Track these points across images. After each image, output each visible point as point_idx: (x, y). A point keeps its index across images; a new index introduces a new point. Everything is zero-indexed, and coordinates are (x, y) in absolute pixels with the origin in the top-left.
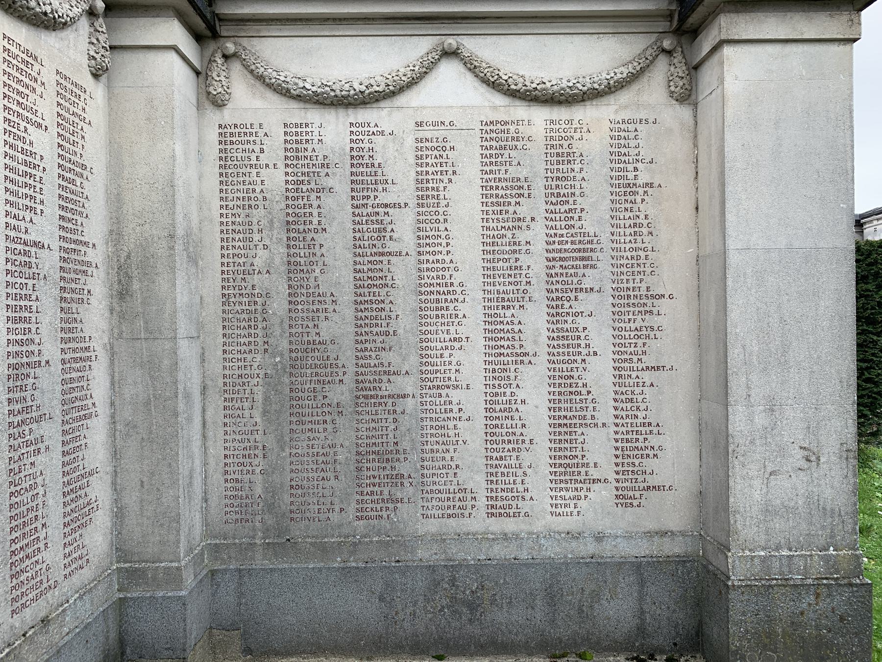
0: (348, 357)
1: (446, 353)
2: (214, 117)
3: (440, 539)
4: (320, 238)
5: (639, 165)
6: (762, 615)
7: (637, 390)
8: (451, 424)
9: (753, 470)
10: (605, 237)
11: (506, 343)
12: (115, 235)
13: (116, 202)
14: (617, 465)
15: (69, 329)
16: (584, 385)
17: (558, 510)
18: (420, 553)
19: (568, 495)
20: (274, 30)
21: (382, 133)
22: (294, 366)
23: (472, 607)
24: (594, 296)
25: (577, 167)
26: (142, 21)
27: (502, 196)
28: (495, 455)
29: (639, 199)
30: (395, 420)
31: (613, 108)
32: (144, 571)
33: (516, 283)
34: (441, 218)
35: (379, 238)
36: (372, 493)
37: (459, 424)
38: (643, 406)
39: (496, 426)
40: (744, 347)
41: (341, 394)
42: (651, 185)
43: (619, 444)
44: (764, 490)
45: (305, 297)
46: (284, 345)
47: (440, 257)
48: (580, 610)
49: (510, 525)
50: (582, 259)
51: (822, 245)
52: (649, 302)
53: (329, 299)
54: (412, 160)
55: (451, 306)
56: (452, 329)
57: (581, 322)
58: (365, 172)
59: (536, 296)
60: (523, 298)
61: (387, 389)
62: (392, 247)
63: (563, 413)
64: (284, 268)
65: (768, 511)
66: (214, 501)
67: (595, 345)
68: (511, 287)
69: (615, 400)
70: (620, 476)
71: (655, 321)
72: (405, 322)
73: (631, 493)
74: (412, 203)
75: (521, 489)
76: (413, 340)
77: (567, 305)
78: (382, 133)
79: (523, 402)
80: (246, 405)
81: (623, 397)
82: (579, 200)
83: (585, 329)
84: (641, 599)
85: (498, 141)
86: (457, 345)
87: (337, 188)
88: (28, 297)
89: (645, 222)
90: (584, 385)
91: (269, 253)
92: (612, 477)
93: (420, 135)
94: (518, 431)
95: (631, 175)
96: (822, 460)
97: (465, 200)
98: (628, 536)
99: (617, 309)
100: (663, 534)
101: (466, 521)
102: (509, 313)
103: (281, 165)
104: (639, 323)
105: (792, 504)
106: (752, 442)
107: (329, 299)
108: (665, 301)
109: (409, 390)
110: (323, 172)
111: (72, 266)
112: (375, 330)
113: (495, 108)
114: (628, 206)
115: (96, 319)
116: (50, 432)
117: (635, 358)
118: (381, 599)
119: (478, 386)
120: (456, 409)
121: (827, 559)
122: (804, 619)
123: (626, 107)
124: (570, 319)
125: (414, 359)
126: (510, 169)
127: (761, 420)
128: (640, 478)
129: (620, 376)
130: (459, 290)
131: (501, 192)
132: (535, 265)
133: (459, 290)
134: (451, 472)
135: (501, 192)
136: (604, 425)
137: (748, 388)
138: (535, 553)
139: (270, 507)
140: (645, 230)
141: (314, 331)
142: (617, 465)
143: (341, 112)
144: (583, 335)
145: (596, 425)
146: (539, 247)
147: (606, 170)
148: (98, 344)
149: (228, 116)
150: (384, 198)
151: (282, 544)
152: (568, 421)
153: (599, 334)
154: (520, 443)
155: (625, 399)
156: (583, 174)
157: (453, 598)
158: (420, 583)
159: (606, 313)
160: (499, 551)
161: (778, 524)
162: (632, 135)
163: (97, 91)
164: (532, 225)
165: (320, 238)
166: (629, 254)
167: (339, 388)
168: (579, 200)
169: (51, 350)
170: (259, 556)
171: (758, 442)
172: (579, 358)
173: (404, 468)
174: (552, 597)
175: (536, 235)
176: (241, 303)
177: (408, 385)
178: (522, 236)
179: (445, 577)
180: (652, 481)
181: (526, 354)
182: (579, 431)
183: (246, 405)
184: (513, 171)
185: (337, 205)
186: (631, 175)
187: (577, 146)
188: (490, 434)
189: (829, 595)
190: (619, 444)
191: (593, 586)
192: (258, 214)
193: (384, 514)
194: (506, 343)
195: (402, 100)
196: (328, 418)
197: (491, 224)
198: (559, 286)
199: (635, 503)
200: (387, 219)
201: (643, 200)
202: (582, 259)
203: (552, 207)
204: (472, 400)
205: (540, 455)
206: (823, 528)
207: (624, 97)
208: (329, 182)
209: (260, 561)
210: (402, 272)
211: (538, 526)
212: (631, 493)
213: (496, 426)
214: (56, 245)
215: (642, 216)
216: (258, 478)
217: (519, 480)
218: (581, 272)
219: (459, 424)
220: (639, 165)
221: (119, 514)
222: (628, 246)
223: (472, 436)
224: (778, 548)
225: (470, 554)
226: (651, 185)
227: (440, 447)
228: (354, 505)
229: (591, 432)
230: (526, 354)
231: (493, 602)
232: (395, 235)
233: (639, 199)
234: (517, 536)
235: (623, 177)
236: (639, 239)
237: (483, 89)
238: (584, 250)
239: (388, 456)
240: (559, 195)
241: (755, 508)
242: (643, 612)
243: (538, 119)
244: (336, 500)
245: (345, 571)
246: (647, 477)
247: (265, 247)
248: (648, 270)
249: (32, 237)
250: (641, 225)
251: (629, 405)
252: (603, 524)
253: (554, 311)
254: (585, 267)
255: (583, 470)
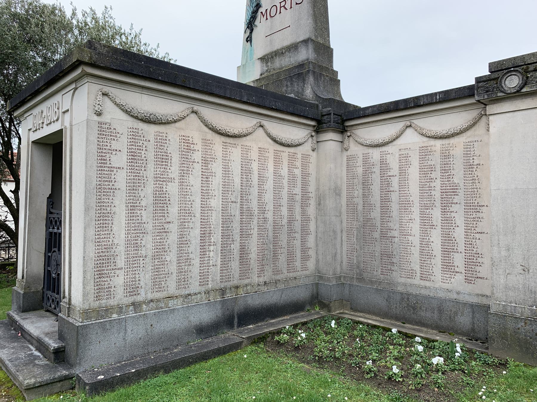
0: (378, 224)
1: (408, 224)
2: (346, 154)
3: (405, 285)
4: (371, 187)
5: (475, 157)
6: (501, 326)
7: (474, 241)
8: (409, 247)
9: (501, 271)
10: (462, 185)
11: (427, 221)
12: (318, 189)
13: (318, 180)
14: (465, 267)
15: (304, 213)
16: (454, 238)
17: (444, 281)
18: (399, 288)
19: (447, 276)
20: (360, 127)
21: (389, 154)
22: (364, 226)
23: (414, 309)
24: (458, 205)
25: (451, 160)
26: (324, 134)
27: (426, 171)
28: (423, 259)
29: (474, 170)
30: (392, 245)
31: (465, 137)
32: (323, 277)
33: (430, 201)
34: (406, 179)
35: (388, 186)
36: (385, 267)
37: (412, 248)
38: (476, 247)
39: (423, 250)
40: (497, 225)
41: (377, 235)
42: (479, 165)
43: (466, 260)
44: (505, 280)
45: (368, 206)
46: (362, 219)
47: (405, 192)
48: (450, 318)
49: (428, 284)
50: (453, 192)
51: (530, 187)
52: (478, 208)
53: (373, 206)
54: (398, 161)
55: (409, 208)
56: (409, 216)
57: (453, 215)
58: (384, 165)
59: (437, 205)
60: (433, 206)
61: (390, 234)
62: (391, 189)
63: (446, 247)
64: (362, 196)
65: (506, 287)
66: (344, 263)
67: (458, 223)
68: (429, 202)
69: (465, 244)
70: (466, 272)
71: (480, 215)
72: (395, 213)
73: (471, 279)
74: (398, 175)
75: (431, 272)
76: (398, 219)
77: (448, 208)
78: (389, 154)
79: (432, 242)
80: (352, 236)
81: (468, 243)
82: (452, 171)
83: (454, 217)
84: (473, 318)
85: (425, 153)
86: (411, 221)
87: (376, 172)
88: (292, 206)
89: (477, 178)
90: (454, 238)
91: (358, 192)
92: (464, 272)
93: (400, 153)
94: (431, 252)
95: (471, 161)
96: (530, 271)
97: (414, 173)
98: (470, 294)
99: (466, 210)
100: (483, 296)
101: (413, 280)
102: (428, 211)
103: (362, 166)
104: (474, 216)
105: (517, 287)
106: (501, 261)
107: (373, 206)
108: (485, 208)
109: (396, 235)
110: (373, 167)
111: (305, 198)
112: (386, 215)
113: (424, 142)
114: (470, 172)
115: (311, 210)
116: (298, 236)
117: (473, 229)
118: (387, 300)
119: (418, 236)
120: (410, 243)
121: (532, 310)
122: (520, 331)
123: (469, 137)
124: (449, 214)
125: (398, 225)
126: (429, 162)
127: (504, 253)
128: (475, 273)
129: (467, 235)
130: (412, 203)
131: (425, 170)
132: (437, 194)
133: (412, 203)
134: (409, 263)
135: (425, 170)
136: (461, 252)
137: (498, 240)
138: (435, 295)
139: (358, 267)
140: (477, 181)
141: (369, 215)
142: (465, 267)
143: (378, 148)
144: (453, 219)
145: (458, 252)
146: (438, 188)
147: (462, 160)
148: (312, 217)
149: (349, 153)
150: (389, 174)
151: (361, 279)
152: (448, 250)
153: (459, 219)
154: (431, 256)
155: (469, 244)
156: (454, 162)
157: (408, 304)
158: (398, 297)
159: (462, 212)
160: (424, 292)
161: (511, 293)
162: (472, 147)
163: (314, 154)
164: (436, 180)
165: (371, 187)
166: (471, 190)
167: (376, 233)
168: (452, 171)
169: (298, 217)
170: (355, 281)
171: (503, 261)
172: (452, 228)
173: (394, 260)
174: (441, 311)
175: (437, 184)
176: (352, 207)
177: (396, 233)
178: (432, 185)
179: (405, 297)
180: (479, 275)
181: (434, 225)
182: (452, 254)
183: (352, 236)
184: (430, 163)
185: (376, 178)
186: (471, 161)
187: (452, 152)
188: (421, 252)
189: (531, 324)
190: (466, 260)
191: (455, 310)
192: (356, 180)
193: (389, 274)
194: (427, 221)
195: (395, 143)
196: (373, 242)
197: (422, 181)
198: (445, 202)
199: (473, 282)
200: (390, 180)
201: (476, 170)
202: (453, 192)
203: (443, 174)
204: (415, 240)
205: (438, 261)
206: (530, 298)
207: (469, 133)
208: (374, 170)
209: (355, 283)
210: (394, 197)
211: (437, 286)
212: (471, 279)
213: (423, 250)
214: (300, 194)
215: (476, 176)
216: (355, 258)
217: (431, 269)
218: (453, 197)
219: (412, 248)
220: (475, 157)
221: (317, 261)
222: (470, 187)
223: (415, 251)
224: (511, 303)
225: (414, 291)
226: (479, 165)
227: (406, 255)
228: (380, 270)
229: (456, 255)
230: (434, 225)
231: (420, 308)
232: (392, 185)
233: (474, 170)
234: (429, 288)
235: (468, 162)
236: (475, 184)
237: (420, 136)
238: (454, 189)
239: (390, 256)
240: (445, 170)
241: (501, 286)
242: (474, 323)
243: (438, 143)
244: (375, 268)
245: (377, 290)
246: (477, 273)
247: (357, 190)
248: (478, 196)
249: (294, 193)
250: (475, 180)
251: (470, 246)
252: (460, 289)
253: (443, 211)
254: (454, 195)
255: (453, 268)
